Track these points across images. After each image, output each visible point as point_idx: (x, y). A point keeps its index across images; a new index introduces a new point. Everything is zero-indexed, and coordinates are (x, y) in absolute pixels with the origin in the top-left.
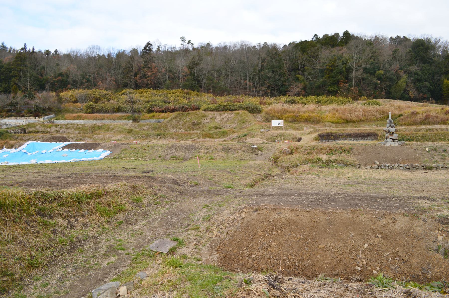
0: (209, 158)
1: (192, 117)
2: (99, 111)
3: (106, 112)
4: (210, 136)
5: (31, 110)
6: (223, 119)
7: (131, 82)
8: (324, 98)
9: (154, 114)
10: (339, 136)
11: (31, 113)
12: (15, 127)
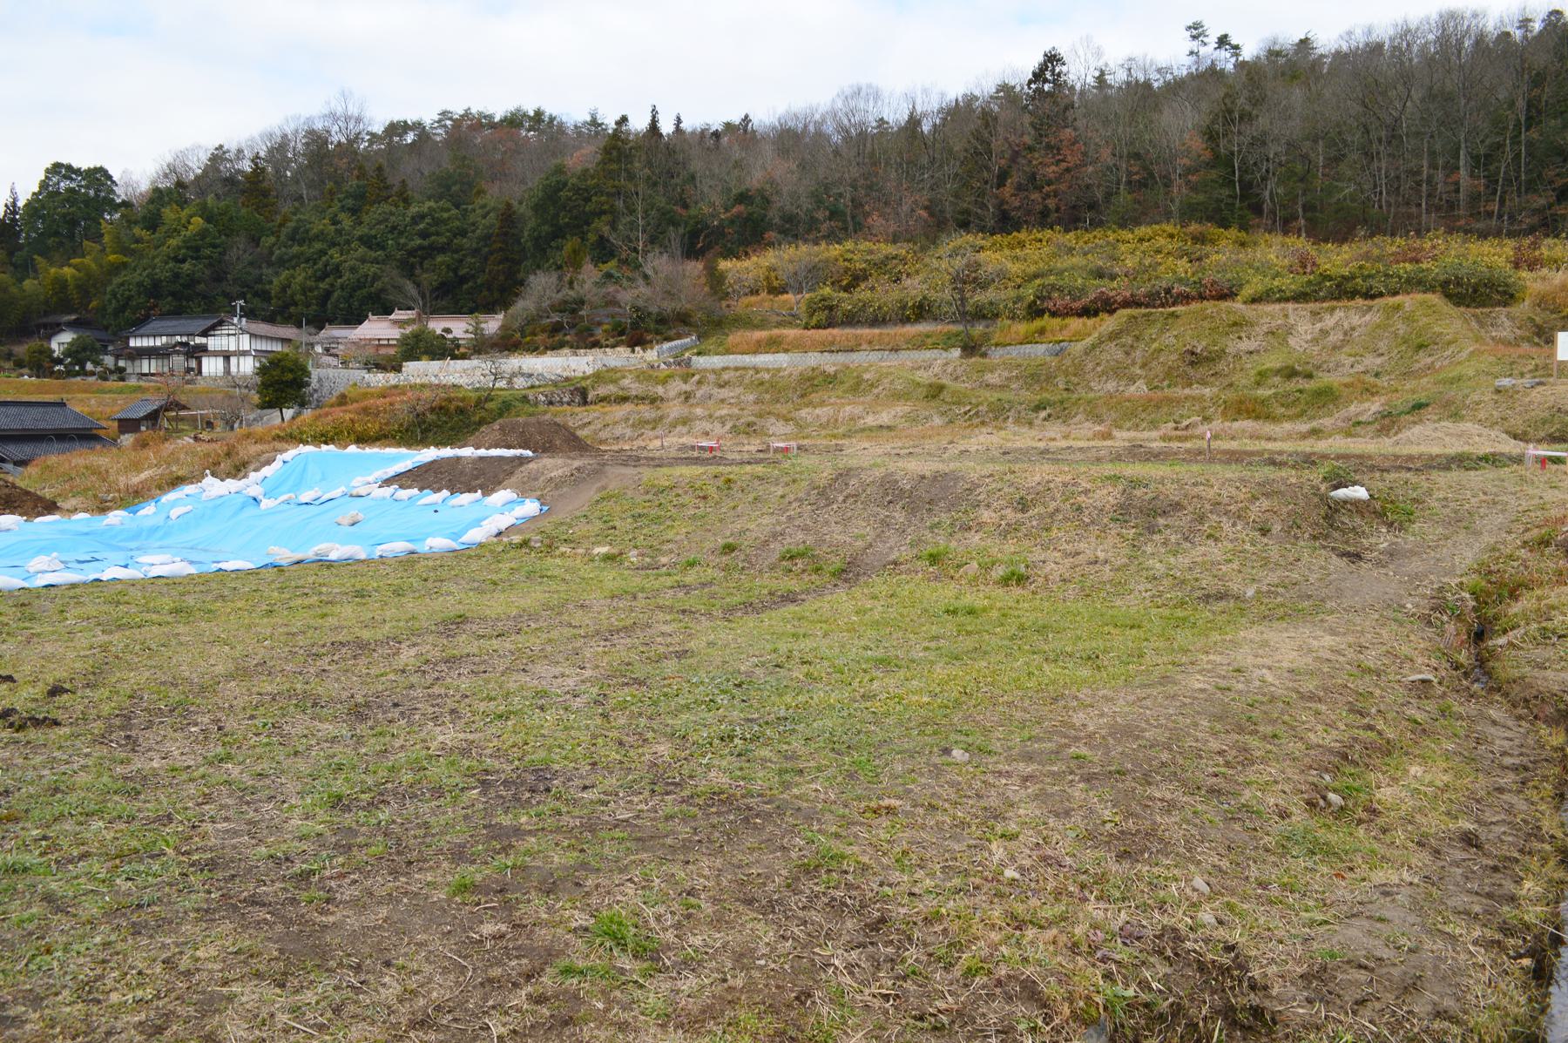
0: (999, 572)
1: (1185, 329)
2: (851, 320)
3: (877, 321)
4: (1255, 410)
5: (619, 324)
6: (1324, 333)
7: (983, 206)
9: (1046, 321)
11: (622, 333)
12: (555, 384)
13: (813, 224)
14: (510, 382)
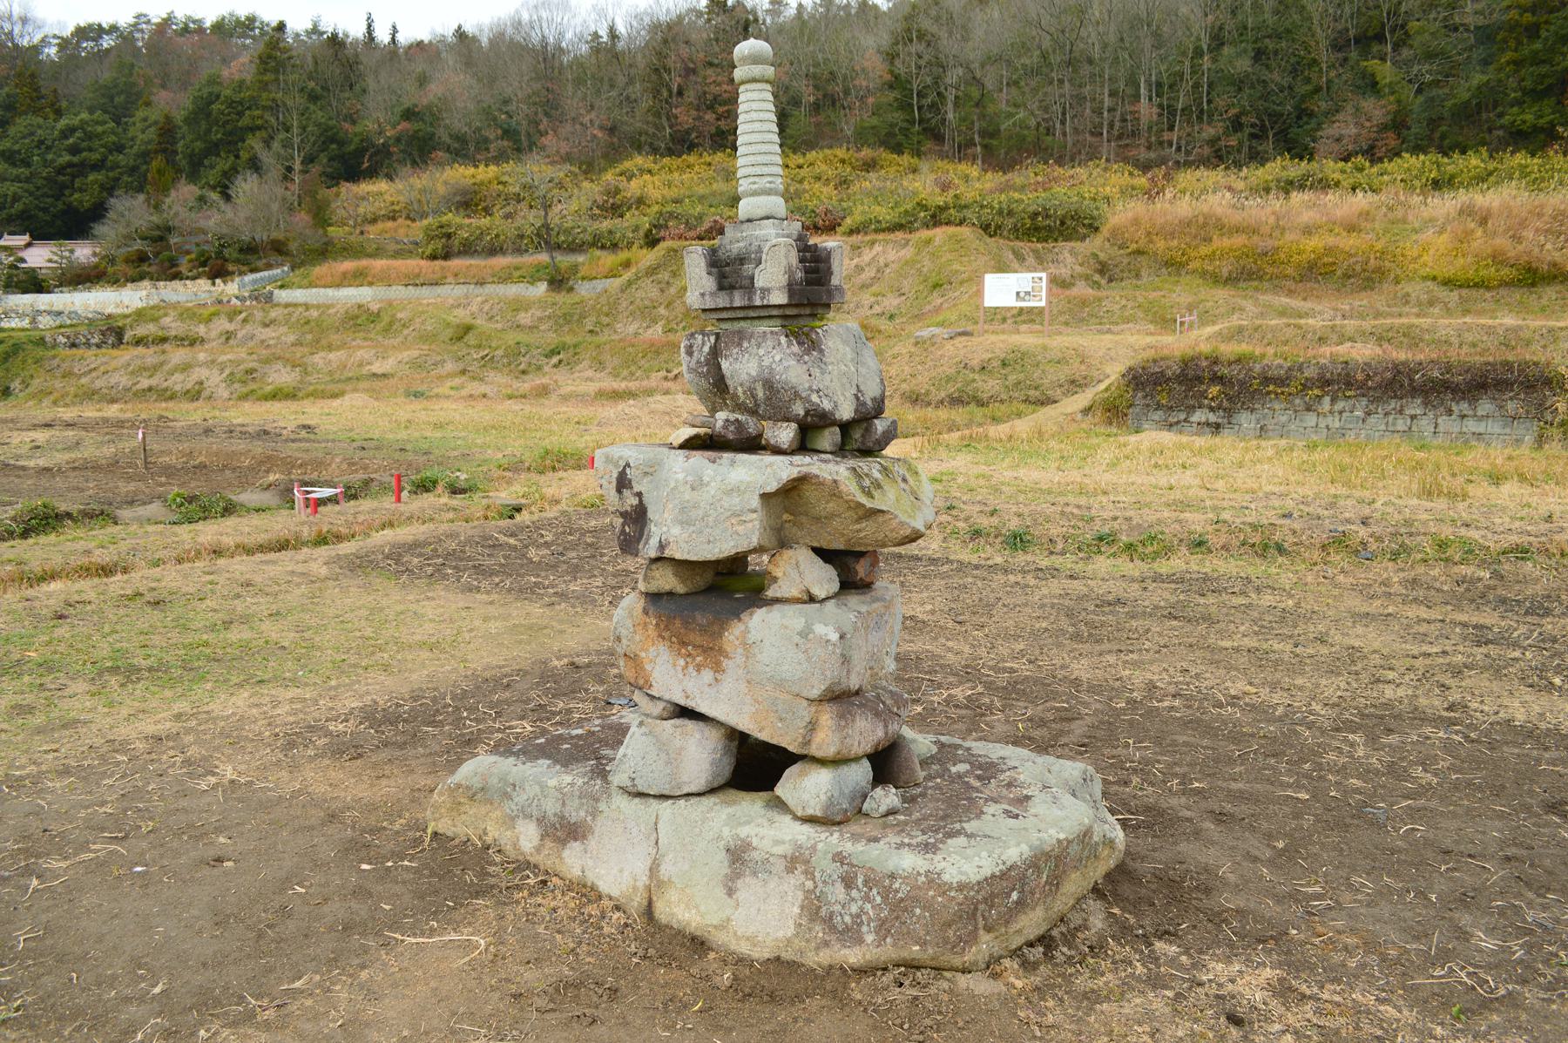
2: (467, 249)
5: (202, 253)
8: (1474, 161)
10: (1267, 380)
11: (204, 264)
13: (483, 144)
14: (33, 321)
